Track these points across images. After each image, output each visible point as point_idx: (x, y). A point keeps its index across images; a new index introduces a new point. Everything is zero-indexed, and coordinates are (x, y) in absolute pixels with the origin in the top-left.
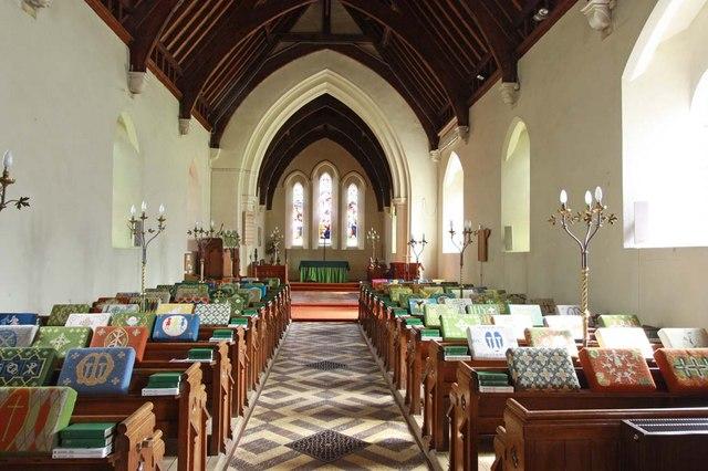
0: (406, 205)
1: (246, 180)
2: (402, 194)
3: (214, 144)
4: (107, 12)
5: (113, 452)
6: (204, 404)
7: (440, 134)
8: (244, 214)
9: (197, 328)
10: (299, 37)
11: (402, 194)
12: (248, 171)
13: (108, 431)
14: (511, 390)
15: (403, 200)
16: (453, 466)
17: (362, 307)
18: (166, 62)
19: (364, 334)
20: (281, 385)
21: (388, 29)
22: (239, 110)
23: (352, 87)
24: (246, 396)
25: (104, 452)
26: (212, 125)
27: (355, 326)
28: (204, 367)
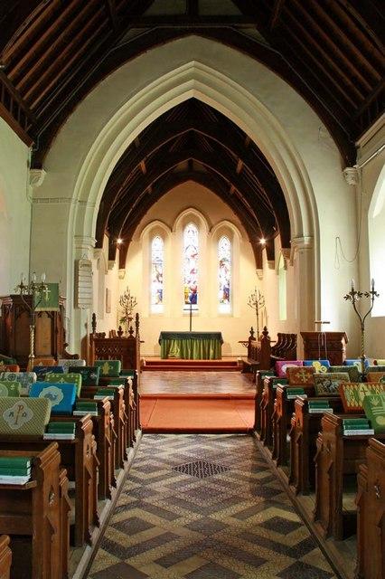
0: (310, 247)
1: (81, 213)
2: (305, 231)
3: (36, 163)
4: (17, 123)
5: (30, 480)
6: (94, 451)
7: (360, 142)
8: (76, 263)
9: (49, 411)
10: (157, 19)
11: (305, 231)
12: (83, 202)
13: (28, 464)
14: (372, 432)
15: (306, 239)
16: (362, 571)
17: (262, 406)
18: (22, 113)
19: (268, 453)
20: (139, 505)
21: (241, 163)
22: (71, 118)
23: (230, 84)
24: (125, 451)
25: (22, 480)
26: (35, 140)
27: (246, 443)
28: (93, 418)
